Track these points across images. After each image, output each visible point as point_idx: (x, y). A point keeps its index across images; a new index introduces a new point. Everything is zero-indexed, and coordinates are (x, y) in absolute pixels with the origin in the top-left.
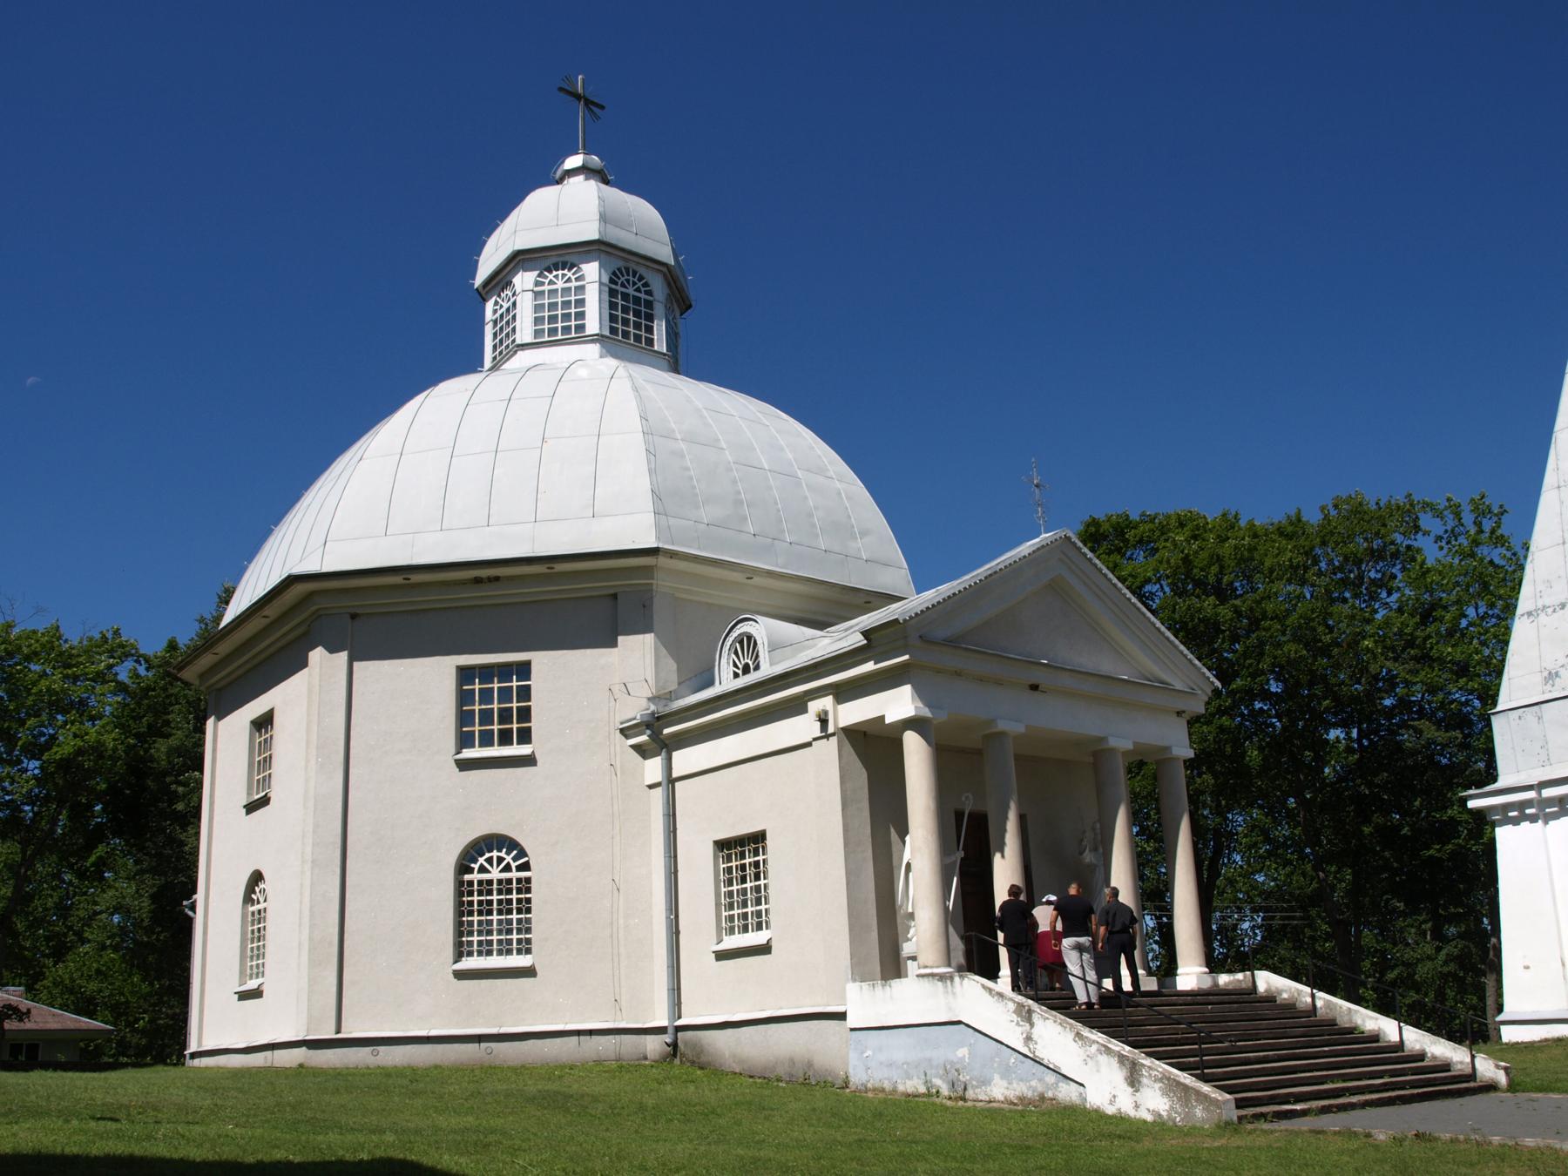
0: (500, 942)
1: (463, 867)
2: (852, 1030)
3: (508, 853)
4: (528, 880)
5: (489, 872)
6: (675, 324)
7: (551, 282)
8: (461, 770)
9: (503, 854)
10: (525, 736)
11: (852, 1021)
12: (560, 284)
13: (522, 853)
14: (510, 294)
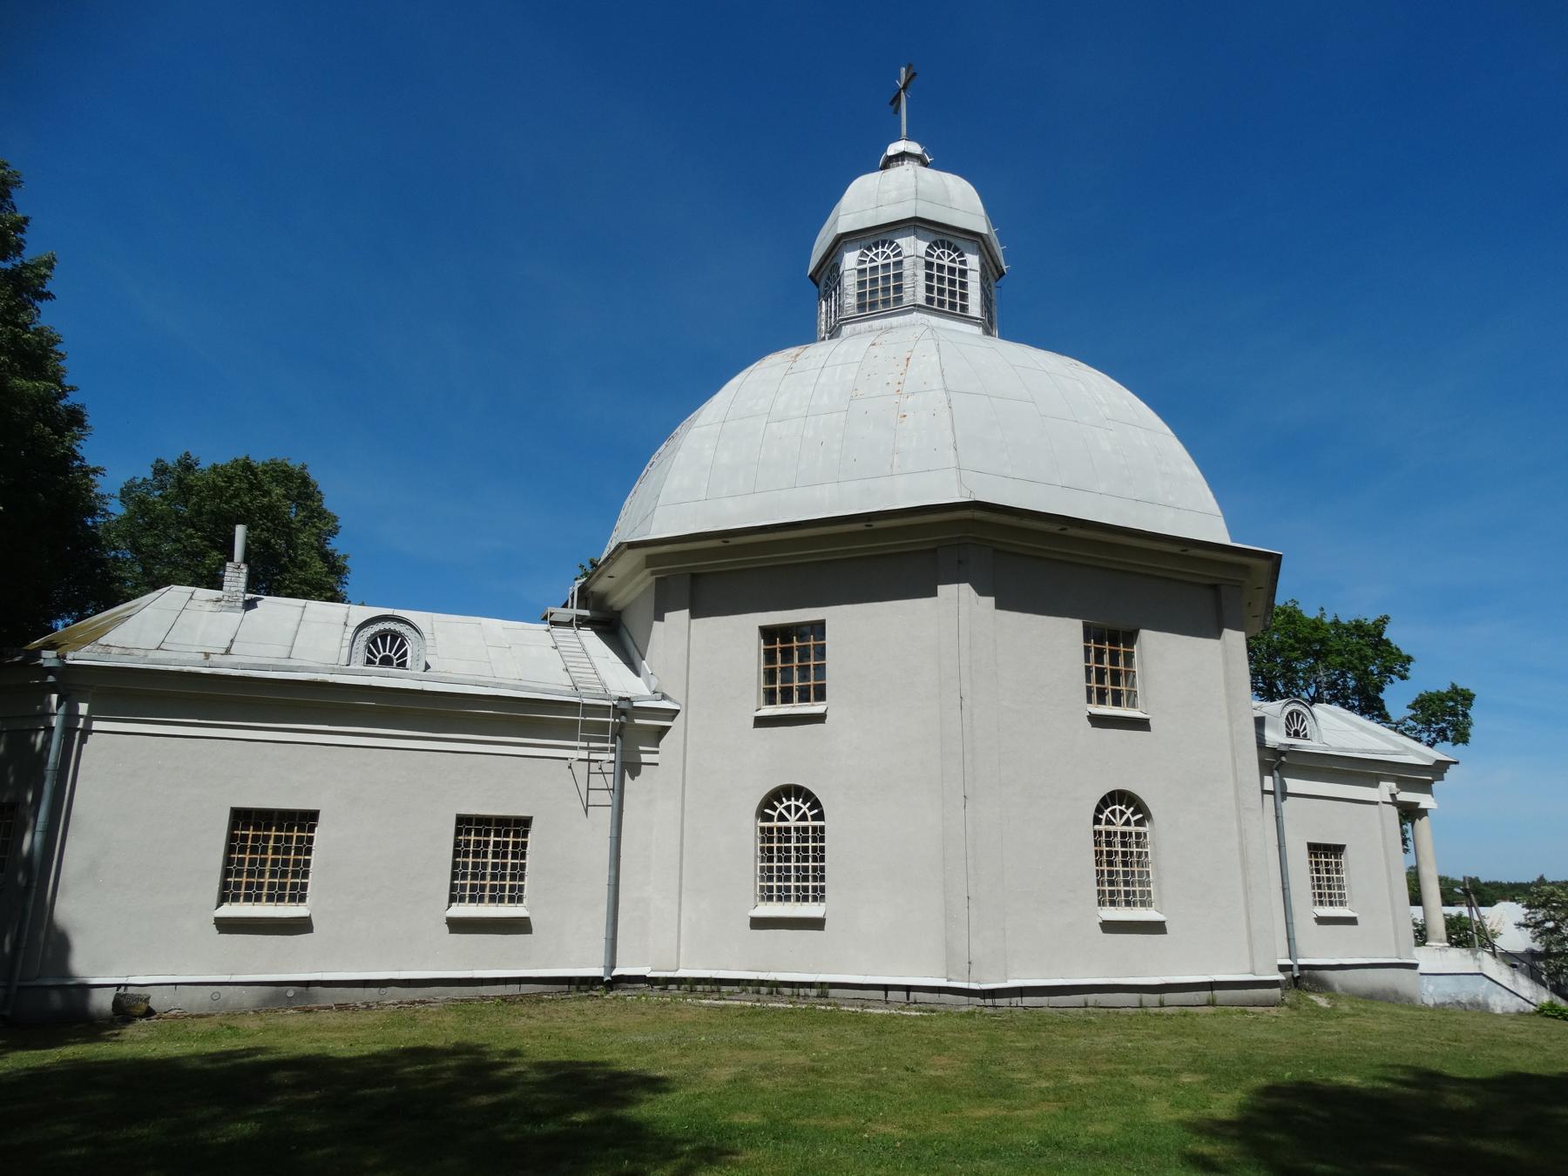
0: (797, 888)
1: (1099, 810)
2: (1422, 974)
3: (804, 803)
4: (822, 829)
5: (788, 820)
6: (990, 291)
7: (872, 260)
8: (1093, 726)
9: (799, 803)
10: (821, 695)
11: (1421, 969)
12: (880, 261)
13: (816, 804)
14: (836, 275)
